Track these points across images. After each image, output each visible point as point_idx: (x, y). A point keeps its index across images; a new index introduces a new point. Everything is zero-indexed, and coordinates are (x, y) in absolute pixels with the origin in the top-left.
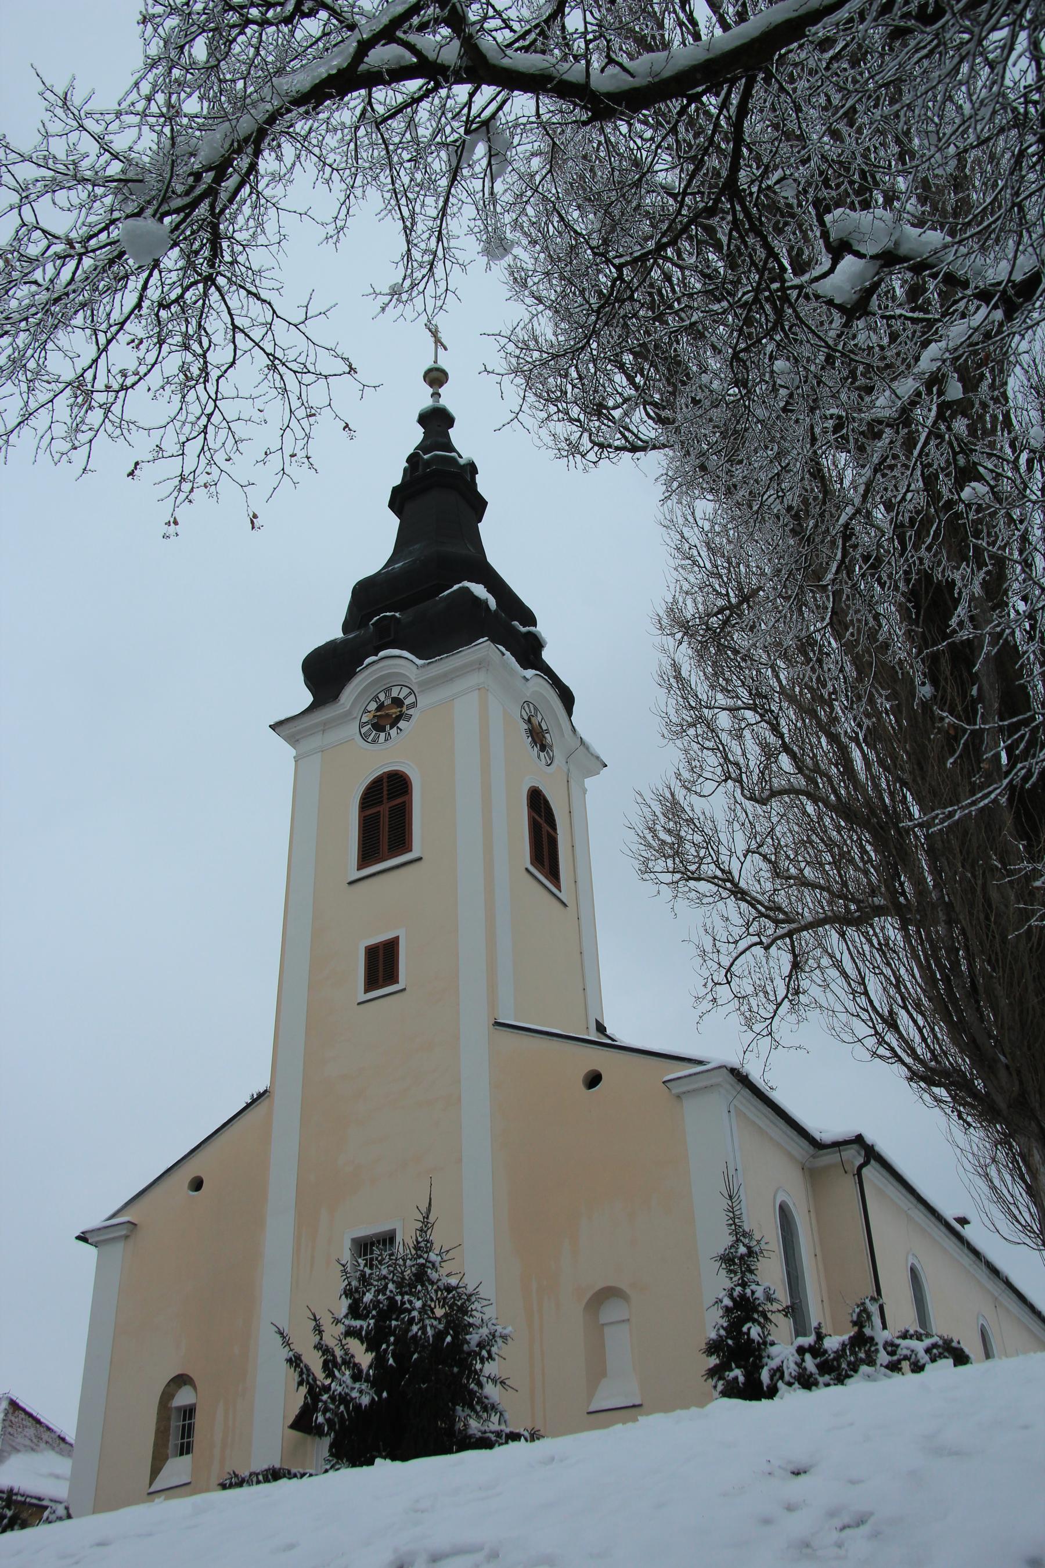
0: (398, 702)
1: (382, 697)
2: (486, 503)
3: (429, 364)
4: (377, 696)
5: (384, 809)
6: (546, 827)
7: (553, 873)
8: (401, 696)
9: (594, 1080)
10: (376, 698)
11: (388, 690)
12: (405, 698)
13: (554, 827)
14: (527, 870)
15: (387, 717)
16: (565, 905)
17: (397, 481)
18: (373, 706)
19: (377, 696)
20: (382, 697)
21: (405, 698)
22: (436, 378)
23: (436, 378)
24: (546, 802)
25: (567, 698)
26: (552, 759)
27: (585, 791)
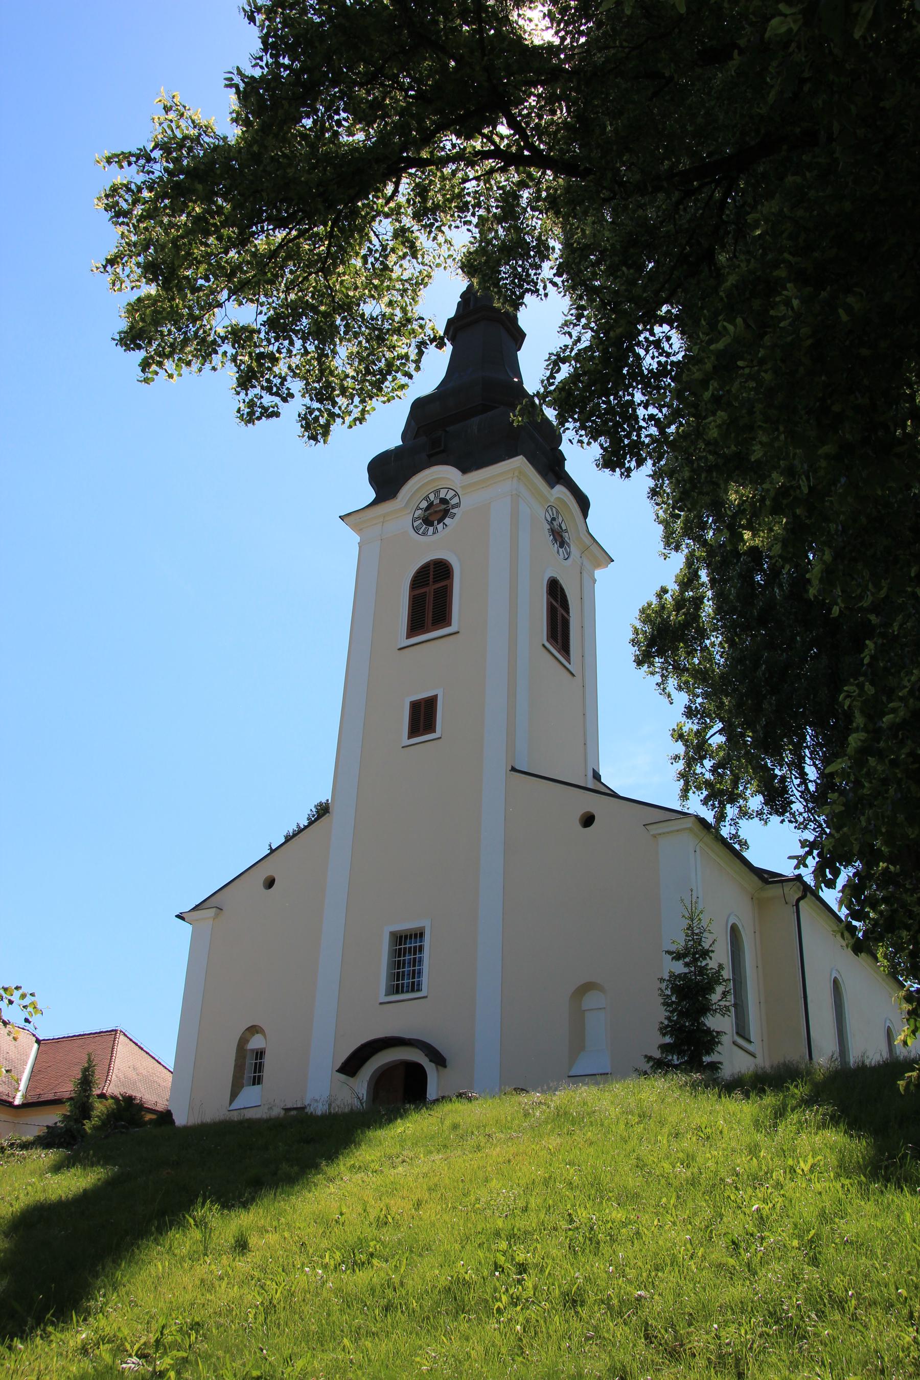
0: (444, 501)
2: (525, 335)
4: (427, 496)
5: (430, 590)
6: (561, 611)
7: (565, 648)
8: (448, 497)
9: (588, 820)
10: (427, 498)
11: (437, 492)
12: (451, 499)
13: (568, 613)
14: (544, 645)
15: (436, 513)
16: (573, 675)
17: (452, 314)
18: (424, 504)
19: (427, 496)
20: (432, 497)
21: (451, 499)
24: (562, 590)
25: (583, 503)
26: (569, 554)
27: (595, 581)
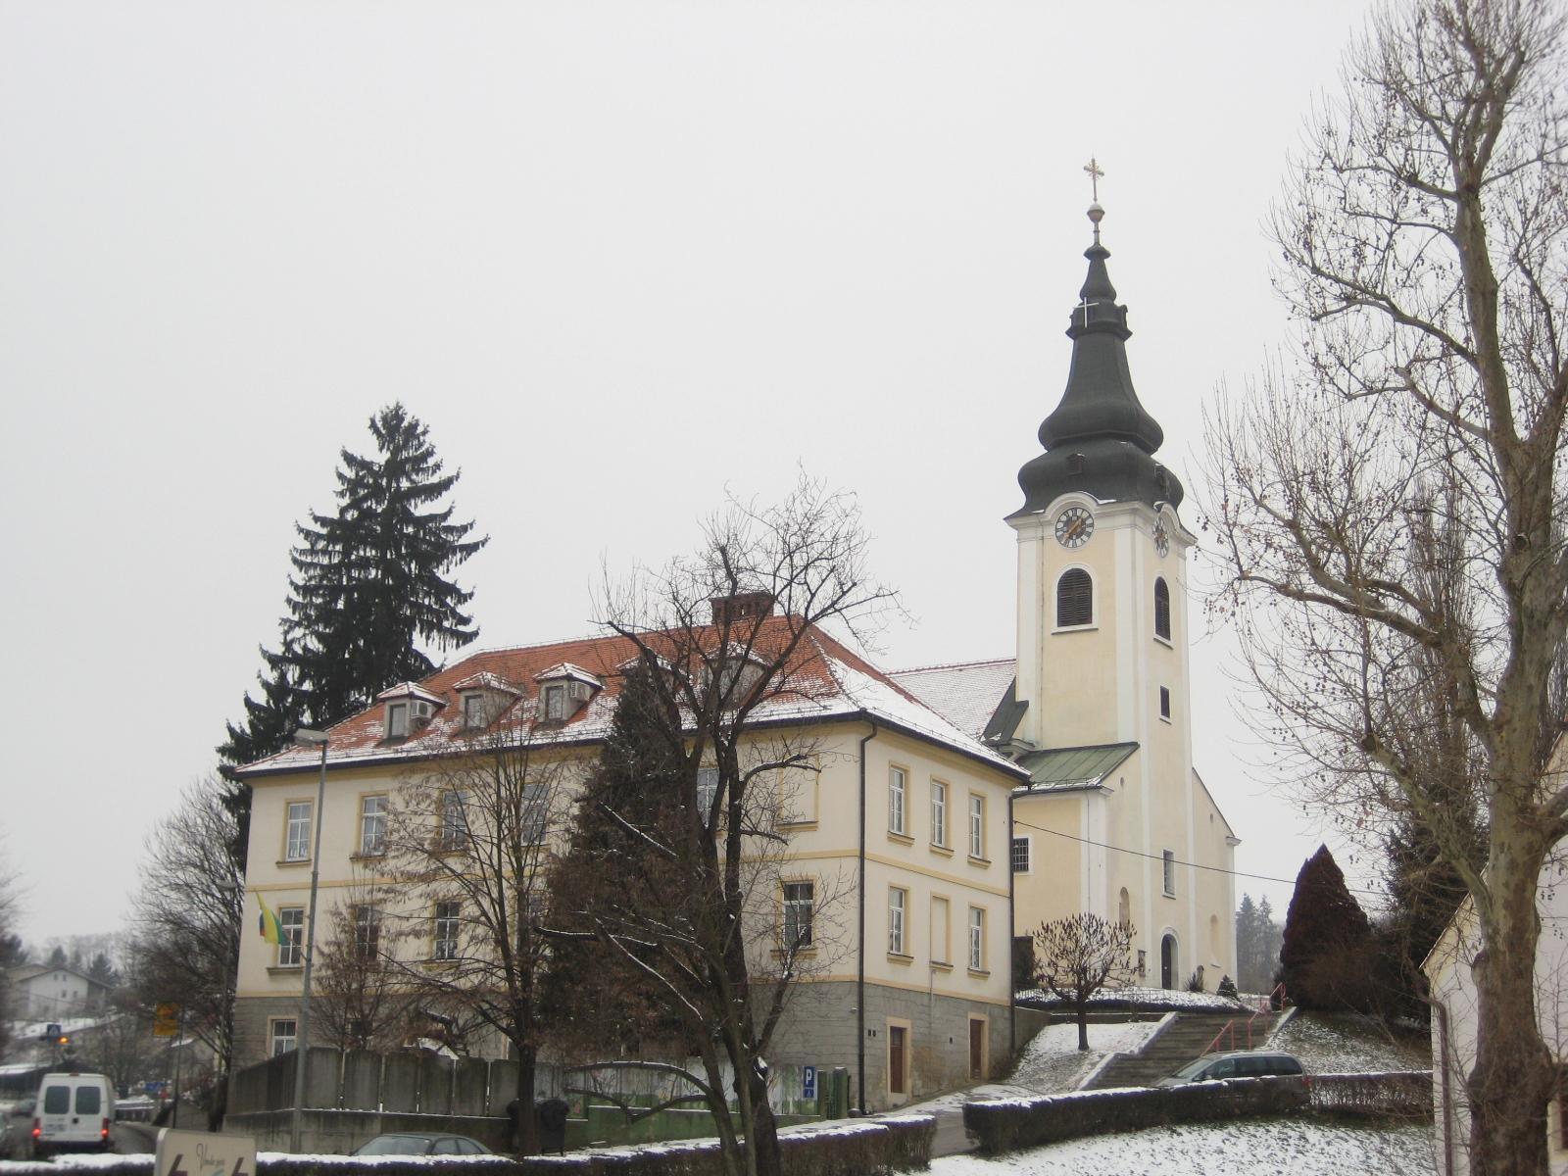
1: (1070, 513)
3: (1090, 243)
15: (1075, 529)
18: (1064, 518)
22: (1096, 215)
23: (1096, 215)
